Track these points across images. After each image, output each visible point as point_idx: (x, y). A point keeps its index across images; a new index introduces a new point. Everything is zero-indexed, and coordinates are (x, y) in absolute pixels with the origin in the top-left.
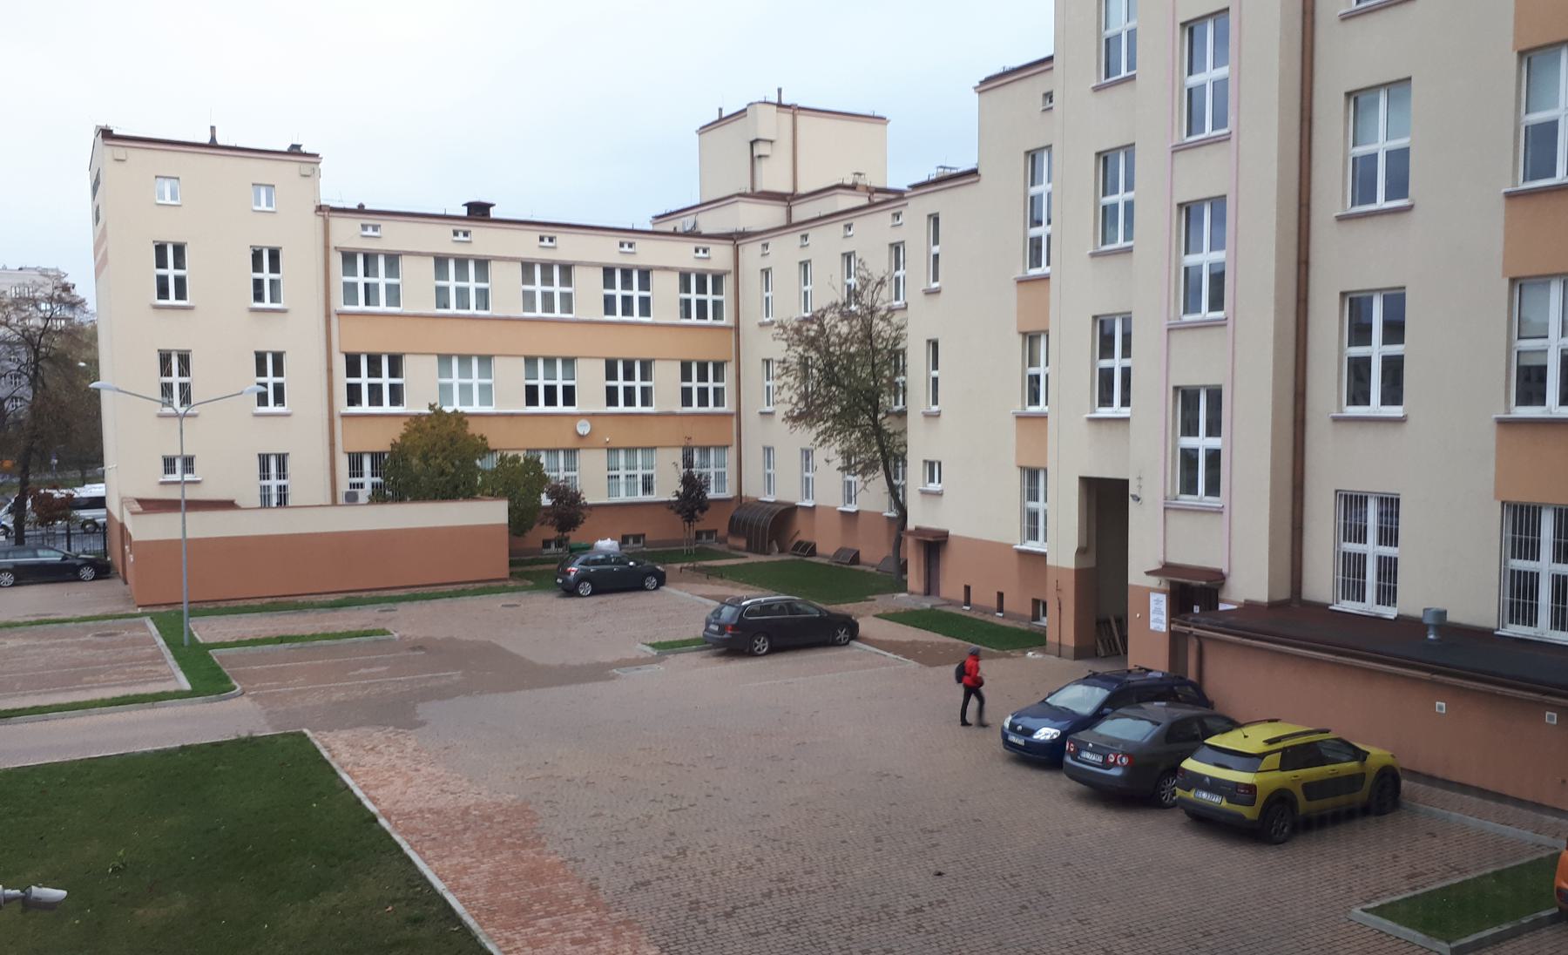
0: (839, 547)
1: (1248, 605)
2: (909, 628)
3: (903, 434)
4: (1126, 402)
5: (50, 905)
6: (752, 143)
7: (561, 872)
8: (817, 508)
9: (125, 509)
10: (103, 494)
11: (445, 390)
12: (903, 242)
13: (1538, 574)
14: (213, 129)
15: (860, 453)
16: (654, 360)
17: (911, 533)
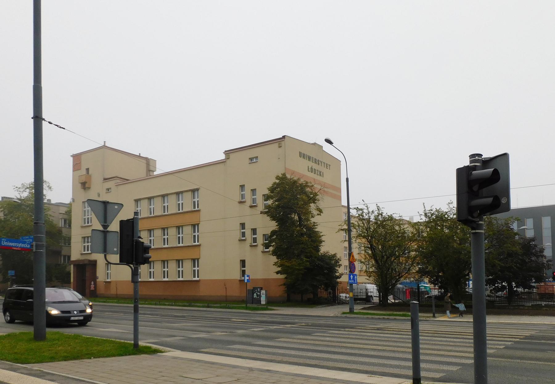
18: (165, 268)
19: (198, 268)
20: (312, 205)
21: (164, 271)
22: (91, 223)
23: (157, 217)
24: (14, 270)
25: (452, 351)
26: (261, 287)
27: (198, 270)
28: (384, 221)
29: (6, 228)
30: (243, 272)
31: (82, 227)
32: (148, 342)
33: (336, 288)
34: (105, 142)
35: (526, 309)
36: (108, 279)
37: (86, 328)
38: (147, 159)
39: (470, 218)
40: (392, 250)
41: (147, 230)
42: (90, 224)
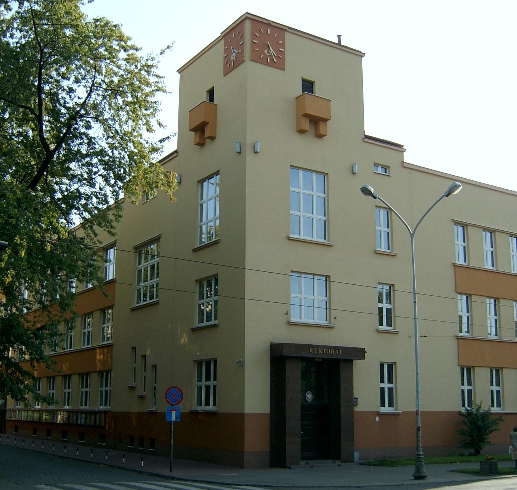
0: (203, 120)
1: (192, 413)
2: (247, 164)
3: (119, 52)
4: (215, 404)
5: (258, 50)
6: (325, 175)
7: (51, 4)
8: (298, 129)
9: (388, 207)
10: (381, 408)
11: (85, 86)
12: (395, 363)
13: (177, 71)
14: (171, 93)
15: (20, 274)
16: (473, 367)
17: (80, 246)
18: (210, 380)
20: (11, 280)
21: (498, 385)
22: (216, 319)
23: (511, 369)
24: (62, 207)
25: (158, 271)
26: (155, 364)
27: (215, 387)
28: (490, 414)
29: (21, 87)
31: (134, 310)
32: (456, 469)
33: (483, 252)
34: (141, 49)
35: (63, 38)
36: (83, 388)
37: (143, 362)
38: (204, 144)
39: (123, 136)
40: (29, 172)
42: (213, 322)
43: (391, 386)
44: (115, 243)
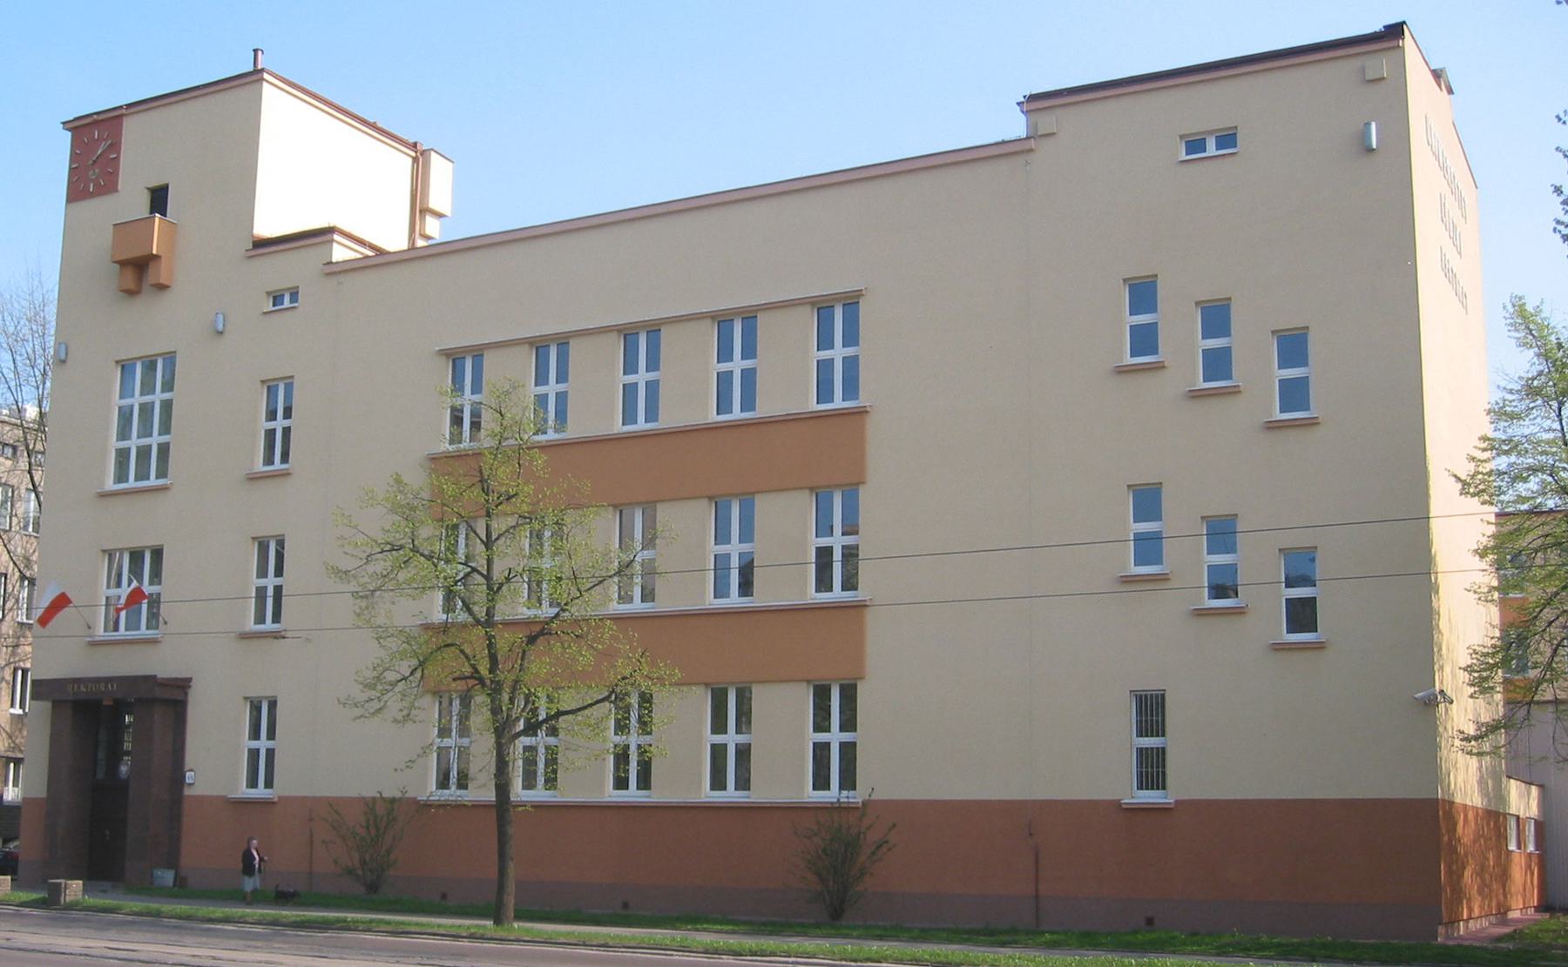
13: (64, 123)
19: (270, 744)
30: (1152, 769)
41: (706, 499)
43: (270, 744)
44: (859, 296)
